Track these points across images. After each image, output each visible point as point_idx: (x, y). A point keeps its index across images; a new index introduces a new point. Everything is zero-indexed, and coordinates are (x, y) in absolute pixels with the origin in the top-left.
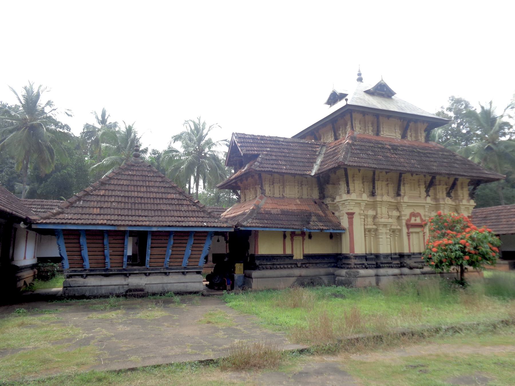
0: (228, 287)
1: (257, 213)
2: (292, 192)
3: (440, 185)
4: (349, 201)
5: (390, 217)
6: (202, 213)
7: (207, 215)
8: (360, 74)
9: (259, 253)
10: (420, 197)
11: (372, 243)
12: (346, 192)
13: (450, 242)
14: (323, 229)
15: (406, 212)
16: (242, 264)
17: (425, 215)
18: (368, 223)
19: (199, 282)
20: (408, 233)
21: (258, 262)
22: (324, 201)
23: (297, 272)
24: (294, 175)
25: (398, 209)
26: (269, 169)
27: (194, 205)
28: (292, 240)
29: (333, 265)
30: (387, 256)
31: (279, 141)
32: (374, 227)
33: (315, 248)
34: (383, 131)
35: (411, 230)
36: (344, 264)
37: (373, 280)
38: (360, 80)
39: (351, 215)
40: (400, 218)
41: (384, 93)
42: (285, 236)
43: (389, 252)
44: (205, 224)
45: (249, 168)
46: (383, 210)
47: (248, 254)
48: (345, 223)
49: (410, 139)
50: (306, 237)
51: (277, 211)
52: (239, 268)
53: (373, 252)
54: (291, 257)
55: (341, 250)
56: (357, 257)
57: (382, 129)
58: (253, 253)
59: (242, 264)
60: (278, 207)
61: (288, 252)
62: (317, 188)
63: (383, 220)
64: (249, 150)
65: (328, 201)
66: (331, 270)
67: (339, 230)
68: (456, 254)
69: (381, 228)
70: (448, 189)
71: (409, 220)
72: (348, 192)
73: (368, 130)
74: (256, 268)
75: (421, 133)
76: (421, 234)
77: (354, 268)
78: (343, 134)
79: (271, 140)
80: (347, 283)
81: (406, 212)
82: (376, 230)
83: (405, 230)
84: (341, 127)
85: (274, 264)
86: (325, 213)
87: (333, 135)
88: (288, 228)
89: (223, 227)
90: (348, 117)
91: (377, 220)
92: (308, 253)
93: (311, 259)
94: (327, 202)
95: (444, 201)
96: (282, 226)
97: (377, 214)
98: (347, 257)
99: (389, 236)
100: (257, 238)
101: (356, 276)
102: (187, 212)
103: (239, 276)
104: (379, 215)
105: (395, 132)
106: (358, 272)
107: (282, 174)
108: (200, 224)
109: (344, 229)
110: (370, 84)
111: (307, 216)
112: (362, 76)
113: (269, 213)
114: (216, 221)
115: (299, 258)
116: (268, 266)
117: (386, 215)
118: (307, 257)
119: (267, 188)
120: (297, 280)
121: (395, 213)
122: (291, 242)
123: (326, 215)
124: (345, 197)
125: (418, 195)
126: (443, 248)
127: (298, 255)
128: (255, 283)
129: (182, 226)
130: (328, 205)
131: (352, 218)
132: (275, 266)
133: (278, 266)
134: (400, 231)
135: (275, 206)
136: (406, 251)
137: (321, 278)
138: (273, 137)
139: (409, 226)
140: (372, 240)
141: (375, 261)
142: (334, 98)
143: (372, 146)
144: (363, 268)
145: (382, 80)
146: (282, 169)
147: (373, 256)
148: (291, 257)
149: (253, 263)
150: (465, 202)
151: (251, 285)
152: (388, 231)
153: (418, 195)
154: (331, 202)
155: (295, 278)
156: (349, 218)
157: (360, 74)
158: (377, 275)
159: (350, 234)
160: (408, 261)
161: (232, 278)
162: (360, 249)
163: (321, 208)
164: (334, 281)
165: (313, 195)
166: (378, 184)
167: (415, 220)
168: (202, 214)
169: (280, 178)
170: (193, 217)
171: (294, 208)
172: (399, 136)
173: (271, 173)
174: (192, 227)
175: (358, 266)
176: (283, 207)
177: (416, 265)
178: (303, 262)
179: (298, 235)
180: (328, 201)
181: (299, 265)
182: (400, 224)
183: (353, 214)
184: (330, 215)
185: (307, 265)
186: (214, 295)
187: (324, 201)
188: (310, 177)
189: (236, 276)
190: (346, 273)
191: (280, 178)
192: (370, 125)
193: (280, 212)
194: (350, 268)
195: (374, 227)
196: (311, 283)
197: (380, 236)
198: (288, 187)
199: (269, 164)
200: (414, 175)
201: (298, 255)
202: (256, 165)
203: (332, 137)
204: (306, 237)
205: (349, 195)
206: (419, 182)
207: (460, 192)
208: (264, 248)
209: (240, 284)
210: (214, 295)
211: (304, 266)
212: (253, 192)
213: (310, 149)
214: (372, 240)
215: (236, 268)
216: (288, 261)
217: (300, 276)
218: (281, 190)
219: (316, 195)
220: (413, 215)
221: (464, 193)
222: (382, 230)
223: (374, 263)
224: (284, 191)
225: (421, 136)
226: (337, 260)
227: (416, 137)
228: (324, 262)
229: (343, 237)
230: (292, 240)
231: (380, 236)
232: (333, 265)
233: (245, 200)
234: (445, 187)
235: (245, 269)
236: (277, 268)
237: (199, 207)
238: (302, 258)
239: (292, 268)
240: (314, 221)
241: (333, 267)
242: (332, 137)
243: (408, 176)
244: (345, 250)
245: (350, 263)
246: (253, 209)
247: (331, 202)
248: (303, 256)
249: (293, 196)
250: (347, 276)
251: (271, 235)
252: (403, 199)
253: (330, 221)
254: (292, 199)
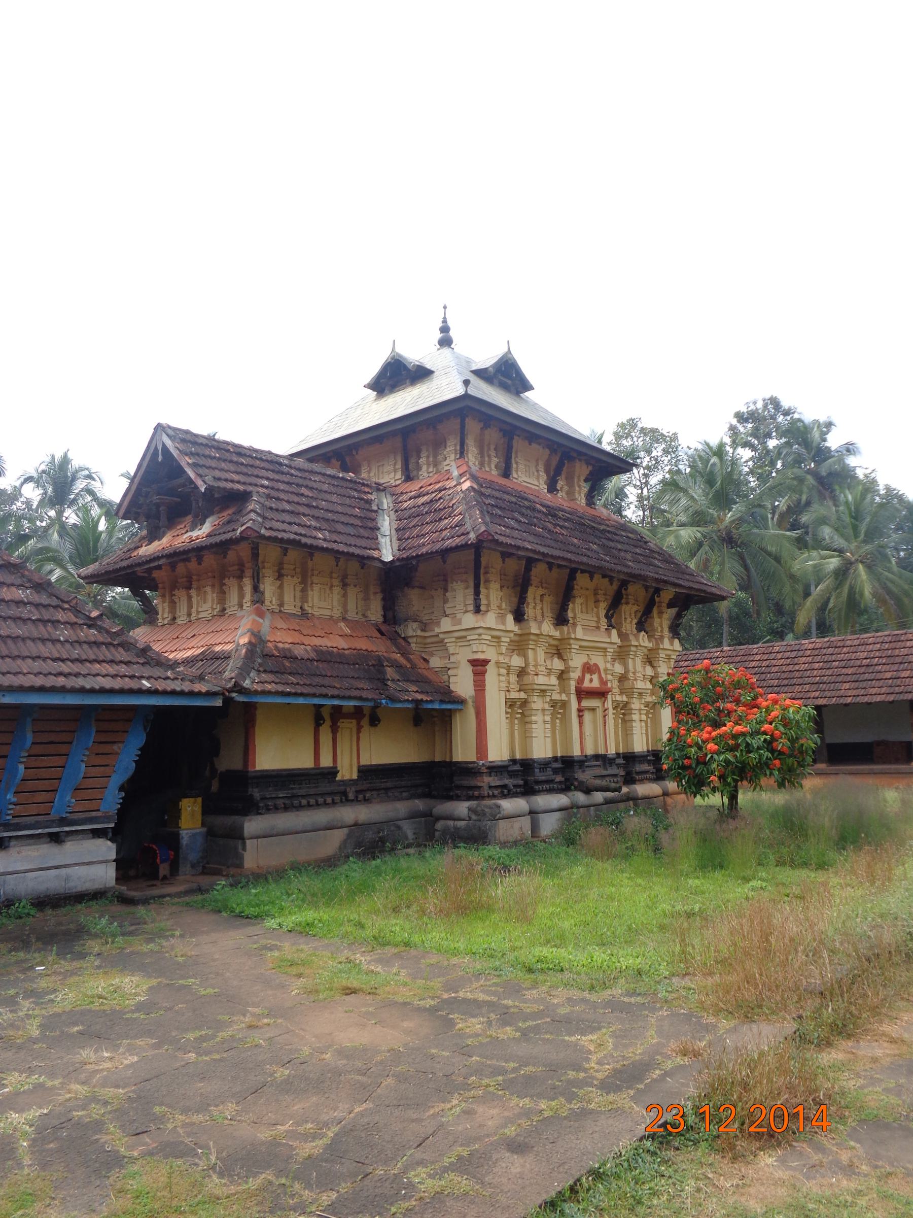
0: (164, 869)
1: (259, 654)
2: (324, 602)
3: (627, 603)
4: (480, 631)
5: (550, 672)
6: (120, 649)
7: (138, 656)
8: (445, 329)
9: (258, 768)
10: (598, 628)
11: (516, 732)
12: (471, 608)
13: (738, 728)
14: (422, 700)
15: (577, 661)
16: (200, 800)
17: (606, 670)
18: (515, 683)
19: (91, 862)
20: (580, 710)
21: (257, 794)
22: (400, 629)
23: (350, 814)
24: (337, 555)
25: (560, 656)
26: (292, 536)
27: (90, 626)
28: (334, 730)
29: (420, 791)
30: (545, 764)
31: (281, 464)
32: (523, 695)
33: (385, 749)
34: (517, 471)
35: (586, 703)
36: (459, 787)
37: (526, 822)
38: (446, 342)
39: (479, 666)
40: (565, 676)
41: (509, 382)
42: (318, 720)
43: (549, 755)
44: (146, 684)
45: (154, 535)
46: (538, 656)
47: (214, 770)
48: (462, 684)
49: (560, 499)
50: (365, 722)
51: (306, 650)
52: (190, 816)
53: (518, 757)
54: (332, 772)
55: (451, 757)
56: (496, 769)
57: (514, 466)
58: (237, 765)
59: (200, 800)
60: (306, 640)
61: (326, 761)
62: (380, 596)
63: (541, 680)
64: (219, 479)
65: (411, 630)
66: (419, 804)
67: (449, 702)
68: (760, 756)
69: (535, 699)
70: (639, 615)
71: (581, 680)
72: (477, 610)
73: (490, 462)
74: (251, 808)
75: (579, 486)
76: (599, 712)
77: (489, 796)
78: (428, 465)
79: (261, 459)
80: (476, 837)
81: (577, 661)
82: (525, 703)
83: (574, 704)
84: (424, 448)
85: (294, 796)
86: (409, 660)
87: (399, 466)
88: (350, 698)
89: (199, 694)
90: (455, 423)
91: (527, 679)
92: (368, 763)
93: (377, 780)
94: (410, 633)
95: (638, 640)
96: (336, 692)
97: (527, 664)
98: (467, 770)
99: (644, 717)
100: (253, 726)
101: (497, 816)
102: (77, 645)
103: (194, 836)
104: (531, 668)
105: (538, 478)
106: (498, 807)
107: (312, 550)
108: (128, 684)
109: (462, 701)
110: (486, 358)
111: (373, 665)
112: (452, 333)
113: (287, 655)
114: (169, 674)
115: (347, 777)
116: (280, 802)
117: (543, 669)
118: (367, 772)
119: (269, 587)
120: (349, 836)
121: (558, 665)
122: (330, 735)
123: (414, 666)
124: (469, 620)
125: (595, 624)
126: (731, 742)
127: (347, 771)
128: (253, 856)
129: (82, 691)
130: (410, 640)
131: (483, 673)
132: (296, 802)
133: (304, 802)
134: (564, 705)
135: (297, 638)
136: (576, 752)
137: (399, 828)
138: (262, 451)
139: (582, 693)
140: (516, 727)
141: (524, 776)
142: (396, 375)
143: (484, 504)
144: (504, 796)
145: (509, 352)
146: (315, 538)
147: (517, 767)
148: (332, 772)
149: (240, 794)
150: (666, 644)
151: (241, 858)
152: (547, 706)
153: (595, 624)
154: (419, 633)
155: (346, 830)
156: (475, 674)
157: (445, 329)
158: (532, 812)
159: (477, 717)
160: (585, 776)
161: (173, 841)
162: (498, 751)
163: (397, 647)
164: (432, 834)
165: (369, 614)
166: (532, 593)
167: (591, 681)
168: (121, 654)
169: (301, 559)
170: (99, 662)
171: (342, 644)
172: (544, 487)
173: (285, 545)
174: (111, 692)
175: (496, 792)
176: (317, 642)
177: (598, 782)
178: (359, 788)
179: (348, 716)
180: (411, 630)
181: (351, 796)
182: (564, 689)
183: (485, 662)
184: (421, 664)
185: (368, 795)
186: (164, 896)
187: (400, 629)
188: (379, 565)
189: (185, 835)
190: (470, 809)
191: (301, 559)
192: (493, 453)
193: (313, 655)
194: (481, 797)
195: (523, 695)
196: (371, 845)
197: (534, 718)
198: (316, 588)
199: (283, 522)
200: (596, 576)
201: (347, 771)
202: (251, 519)
203: (395, 471)
204: (365, 722)
205: (479, 616)
206: (596, 594)
207: (656, 621)
208: (275, 753)
209: (193, 857)
210: (164, 896)
211: (361, 797)
212: (211, 595)
213: (356, 494)
214: (516, 727)
215: (183, 811)
216: (325, 787)
217: (356, 824)
218: (298, 594)
219: (376, 614)
220: (589, 668)
221: (662, 621)
222: (538, 703)
223: (521, 782)
224: (304, 599)
225: (580, 493)
226: (441, 779)
227: (570, 494)
228: (403, 783)
229: (457, 721)
230: (334, 730)
231: (534, 718)
232: (420, 791)
233: (174, 619)
234: (635, 608)
235: (206, 811)
236: (300, 807)
237: (108, 632)
238: (355, 777)
239: (334, 803)
240: (393, 680)
241: (434, 800)
242: (395, 471)
243: (582, 580)
244: (463, 751)
245: (479, 784)
246: (250, 643)
247: (419, 633)
248: (359, 771)
249: (328, 613)
250: (474, 817)
251: (286, 715)
252: (575, 632)
253: (427, 681)
254: (328, 621)
